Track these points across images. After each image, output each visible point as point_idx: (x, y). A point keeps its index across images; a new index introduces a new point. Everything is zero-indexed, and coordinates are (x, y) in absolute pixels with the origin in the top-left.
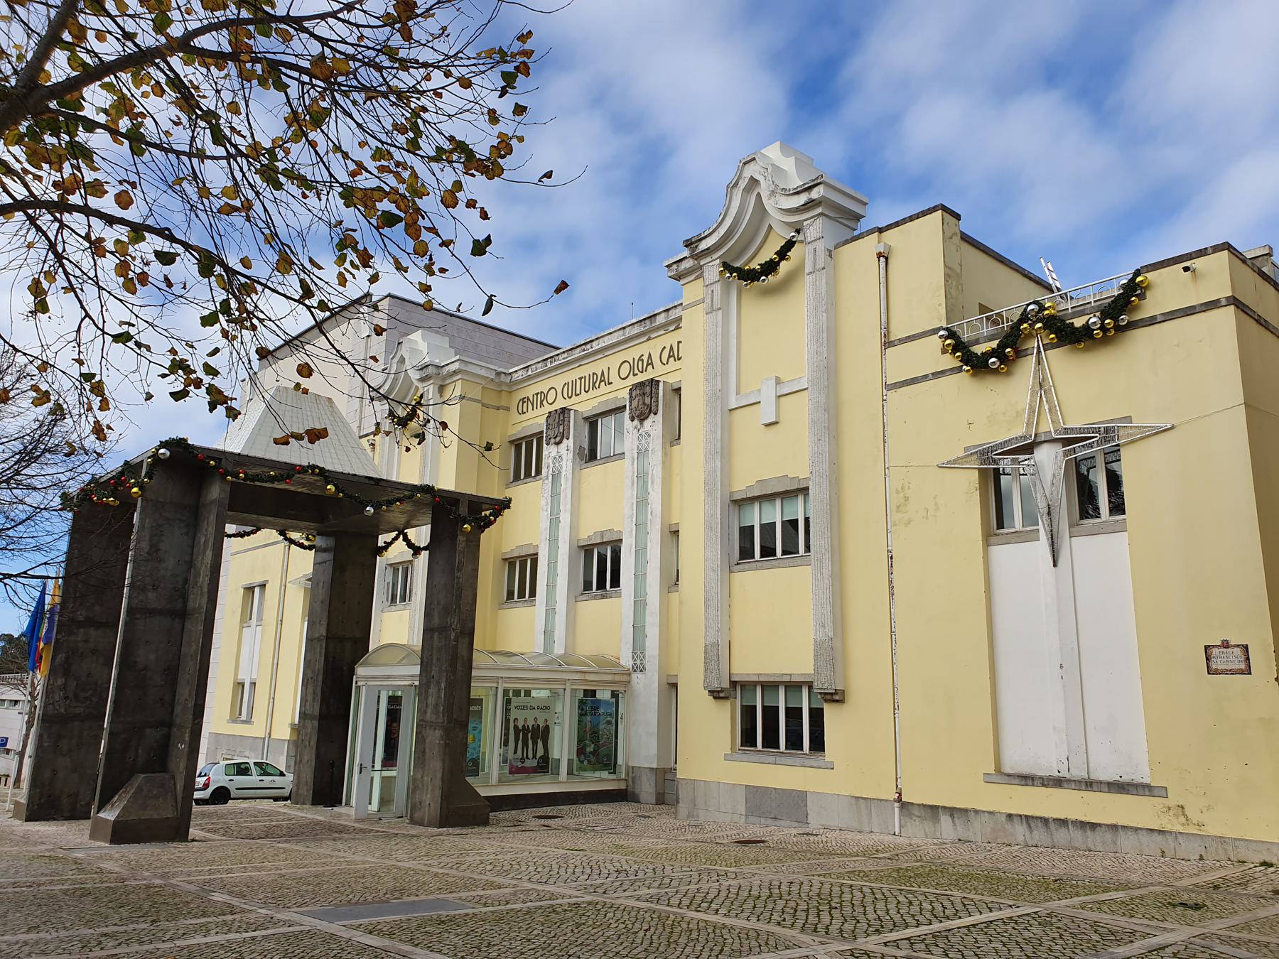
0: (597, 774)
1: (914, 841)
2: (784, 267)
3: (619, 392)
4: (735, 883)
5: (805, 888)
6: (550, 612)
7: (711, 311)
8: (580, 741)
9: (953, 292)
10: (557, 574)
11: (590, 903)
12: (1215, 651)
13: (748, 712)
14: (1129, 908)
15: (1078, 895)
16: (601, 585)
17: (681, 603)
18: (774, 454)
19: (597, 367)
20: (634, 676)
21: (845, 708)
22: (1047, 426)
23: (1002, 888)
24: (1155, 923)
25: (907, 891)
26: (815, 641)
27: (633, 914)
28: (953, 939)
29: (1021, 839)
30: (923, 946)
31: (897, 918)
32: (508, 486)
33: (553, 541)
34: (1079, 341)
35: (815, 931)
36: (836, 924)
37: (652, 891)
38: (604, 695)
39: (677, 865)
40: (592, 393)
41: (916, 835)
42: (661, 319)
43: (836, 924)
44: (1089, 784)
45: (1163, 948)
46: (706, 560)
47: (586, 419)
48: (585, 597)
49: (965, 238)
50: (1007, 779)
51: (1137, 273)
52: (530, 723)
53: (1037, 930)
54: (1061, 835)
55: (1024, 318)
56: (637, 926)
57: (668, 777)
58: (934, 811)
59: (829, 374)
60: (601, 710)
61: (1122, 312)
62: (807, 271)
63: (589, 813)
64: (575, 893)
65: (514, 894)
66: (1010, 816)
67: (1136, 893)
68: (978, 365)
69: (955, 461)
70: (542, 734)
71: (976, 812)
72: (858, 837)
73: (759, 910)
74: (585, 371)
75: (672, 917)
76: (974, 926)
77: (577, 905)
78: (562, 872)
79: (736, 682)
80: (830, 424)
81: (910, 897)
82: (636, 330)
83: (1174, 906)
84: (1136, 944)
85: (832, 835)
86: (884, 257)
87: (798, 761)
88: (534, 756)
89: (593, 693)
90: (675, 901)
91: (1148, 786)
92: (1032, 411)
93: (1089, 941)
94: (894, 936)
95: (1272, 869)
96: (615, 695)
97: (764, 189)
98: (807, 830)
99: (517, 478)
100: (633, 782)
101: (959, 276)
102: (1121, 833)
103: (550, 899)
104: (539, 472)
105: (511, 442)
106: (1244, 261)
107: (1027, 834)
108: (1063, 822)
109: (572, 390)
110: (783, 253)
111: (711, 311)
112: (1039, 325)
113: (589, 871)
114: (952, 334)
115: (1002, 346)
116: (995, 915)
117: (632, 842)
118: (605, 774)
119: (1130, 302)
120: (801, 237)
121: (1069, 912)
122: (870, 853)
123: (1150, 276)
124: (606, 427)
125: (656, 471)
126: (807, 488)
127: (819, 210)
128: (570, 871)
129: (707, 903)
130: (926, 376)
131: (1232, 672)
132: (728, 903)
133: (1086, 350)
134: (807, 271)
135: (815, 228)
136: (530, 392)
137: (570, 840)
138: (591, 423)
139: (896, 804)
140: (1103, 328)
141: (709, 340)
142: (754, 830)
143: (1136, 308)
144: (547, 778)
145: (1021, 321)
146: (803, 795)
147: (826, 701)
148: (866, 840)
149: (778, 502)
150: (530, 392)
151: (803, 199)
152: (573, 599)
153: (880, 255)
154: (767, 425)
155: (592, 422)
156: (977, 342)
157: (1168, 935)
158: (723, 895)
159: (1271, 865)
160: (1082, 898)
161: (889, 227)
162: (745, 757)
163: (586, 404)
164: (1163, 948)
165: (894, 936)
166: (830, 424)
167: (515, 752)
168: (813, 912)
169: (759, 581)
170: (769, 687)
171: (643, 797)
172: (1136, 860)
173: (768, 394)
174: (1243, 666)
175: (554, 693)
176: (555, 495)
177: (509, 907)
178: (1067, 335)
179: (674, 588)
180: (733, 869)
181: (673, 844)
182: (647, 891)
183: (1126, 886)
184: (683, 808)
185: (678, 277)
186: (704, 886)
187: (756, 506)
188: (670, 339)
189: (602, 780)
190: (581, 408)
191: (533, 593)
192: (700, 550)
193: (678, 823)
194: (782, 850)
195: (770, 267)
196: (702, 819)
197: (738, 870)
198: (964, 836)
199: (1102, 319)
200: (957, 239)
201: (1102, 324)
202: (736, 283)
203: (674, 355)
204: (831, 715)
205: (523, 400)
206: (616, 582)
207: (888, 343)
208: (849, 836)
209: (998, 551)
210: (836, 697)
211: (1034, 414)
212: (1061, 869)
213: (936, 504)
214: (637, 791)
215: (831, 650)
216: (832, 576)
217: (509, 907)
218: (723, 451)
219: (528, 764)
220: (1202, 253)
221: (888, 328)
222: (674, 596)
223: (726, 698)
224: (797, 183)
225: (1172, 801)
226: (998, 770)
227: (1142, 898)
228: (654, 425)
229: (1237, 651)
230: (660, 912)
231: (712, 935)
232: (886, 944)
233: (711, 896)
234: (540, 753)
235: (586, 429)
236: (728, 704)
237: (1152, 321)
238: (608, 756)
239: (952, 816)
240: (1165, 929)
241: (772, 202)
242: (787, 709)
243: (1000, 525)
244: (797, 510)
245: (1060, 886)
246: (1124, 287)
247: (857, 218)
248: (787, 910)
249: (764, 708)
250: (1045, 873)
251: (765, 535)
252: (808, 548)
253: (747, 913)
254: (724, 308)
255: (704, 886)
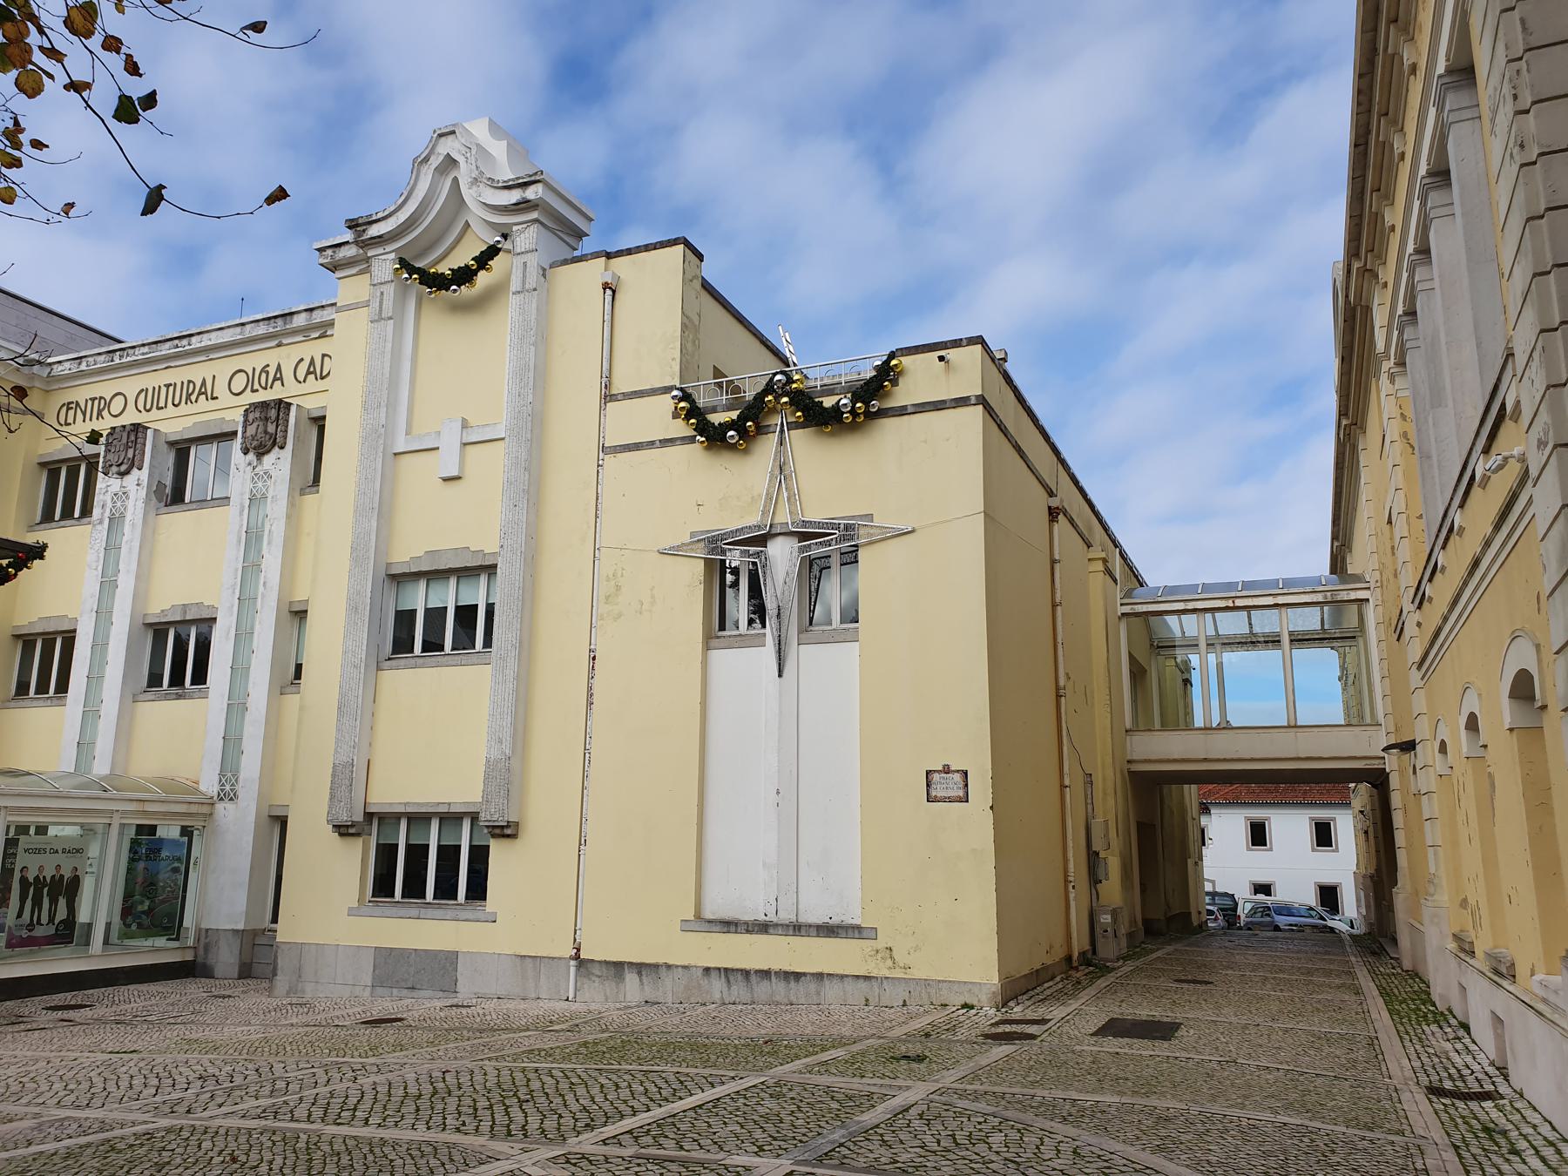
0: (149, 942)
1: (593, 1007)
2: (483, 278)
3: (229, 411)
4: (379, 1078)
5: (478, 1078)
6: (90, 714)
7: (379, 318)
8: (128, 896)
9: (689, 346)
10: (106, 662)
11: (169, 1130)
12: (936, 777)
13: (386, 854)
14: (854, 1065)
15: (797, 1057)
16: (177, 679)
17: (302, 708)
18: (435, 526)
19: (197, 372)
20: (220, 806)
21: (517, 844)
22: (783, 517)
23: (713, 1057)
24: (887, 1081)
25: (607, 1071)
26: (488, 761)
27: (242, 1139)
28: (682, 1127)
29: (717, 996)
30: (649, 1140)
31: (607, 1106)
32: (31, 528)
33: (103, 615)
34: (826, 424)
35: (509, 1134)
36: (534, 1122)
37: (263, 1102)
38: (169, 832)
39: (290, 1061)
40: (190, 408)
41: (595, 998)
42: (300, 321)
43: (534, 1122)
44: (797, 929)
45: (906, 1110)
46: (345, 653)
47: (171, 444)
48: (149, 696)
49: (706, 286)
50: (706, 926)
51: (892, 356)
52: (49, 873)
53: (770, 1104)
54: (762, 989)
55: (769, 388)
56: (254, 1156)
57: (260, 940)
58: (617, 968)
59: (533, 426)
60: (164, 854)
61: (872, 397)
62: (513, 289)
63: (135, 998)
64: (146, 1117)
65: (39, 1127)
66: (707, 970)
67: (855, 1048)
68: (714, 437)
69: (678, 548)
70: (69, 888)
71: (669, 967)
72: (523, 1005)
73: (425, 1114)
74: (178, 375)
75: (304, 1137)
76: (700, 1106)
77: (150, 1135)
78: (111, 1087)
79: (372, 814)
80: (530, 488)
81: (614, 1077)
82: (262, 330)
83: (898, 1060)
84: (880, 1108)
85: (490, 1006)
86: (610, 288)
87: (450, 913)
88: (51, 920)
89: (152, 829)
90: (301, 1112)
91: (858, 928)
92: (769, 497)
93: (830, 1110)
94: (610, 1130)
95: (973, 1012)
96: (187, 832)
97: (464, 174)
98: (455, 1001)
99: (48, 517)
100: (207, 948)
101: (697, 330)
102: (827, 982)
103: (102, 1130)
104: (87, 511)
105: (43, 465)
106: (993, 360)
107: (725, 990)
108: (765, 974)
109: (151, 398)
110: (484, 260)
111: (379, 318)
112: (785, 399)
113: (155, 1082)
114: (686, 396)
115: (743, 418)
116: (719, 1091)
117: (209, 1034)
118: (161, 942)
119: (883, 387)
120: (507, 245)
121: (797, 1078)
122: (545, 1025)
123: (906, 361)
124: (202, 462)
125: (276, 527)
126: (495, 566)
127: (535, 215)
128: (124, 1084)
129: (349, 1111)
130: (652, 443)
131: (951, 800)
132: (378, 1107)
133: (832, 434)
134: (513, 289)
135: (527, 237)
136: (81, 394)
137: (112, 1039)
138: (178, 450)
139: (573, 963)
140: (853, 412)
141: (355, 359)
142: (385, 1005)
143: (887, 395)
144: (64, 951)
145: (766, 392)
146: (451, 958)
147: (494, 836)
148: (535, 1010)
149: (453, 581)
150: (81, 394)
151: (514, 196)
152: (131, 698)
153: (606, 286)
154: (446, 480)
155: (181, 450)
156: (714, 410)
157: (906, 1094)
158: (368, 1098)
159: (972, 1007)
160: (805, 1061)
161: (620, 253)
162: (378, 911)
163: (174, 423)
164: (906, 1110)
165: (610, 1130)
166: (530, 488)
167: (19, 915)
168: (499, 1109)
169: (421, 685)
170: (418, 819)
171: (218, 972)
172: (840, 1011)
173: (450, 441)
174: (961, 793)
175: (88, 830)
176: (111, 548)
177: (34, 1149)
178: (816, 415)
179: (293, 688)
180: (372, 1060)
181: (273, 1032)
182: (256, 1103)
183: (840, 1042)
184: (282, 983)
185: (334, 267)
186: (340, 1088)
187: (422, 584)
188: (313, 349)
189: (159, 950)
190: (165, 428)
191: (63, 687)
192: (335, 639)
193: (275, 1002)
194: (430, 1029)
195: (464, 276)
196: (308, 996)
197: (379, 1062)
198: (652, 998)
199: (854, 402)
200: (697, 284)
201: (853, 407)
202: (417, 287)
203: (316, 371)
204: (499, 853)
205: (68, 406)
206: (200, 676)
207: (608, 397)
208: (511, 1005)
209: (717, 656)
210: (507, 832)
211: (772, 501)
212: (769, 1029)
213: (653, 597)
214: (211, 960)
215: (506, 773)
216: (517, 678)
217: (34, 1149)
218: (381, 508)
219: (39, 932)
220: (956, 344)
221: (609, 377)
222: (292, 701)
223: (358, 835)
224: (507, 174)
225: (881, 943)
226: (698, 916)
227: (863, 1053)
228: (279, 463)
229: (957, 777)
230: (284, 1131)
231: (370, 1158)
232: (604, 1142)
233: (352, 1101)
234: (62, 914)
235: (170, 459)
236: (359, 842)
237: (902, 411)
238: (171, 916)
239: (640, 974)
240: (900, 1088)
241: (473, 191)
242: (440, 847)
243: (722, 627)
244: (476, 594)
245: (771, 1048)
246: (877, 368)
247: (580, 235)
248: (463, 1109)
249: (409, 847)
250: (753, 1034)
251: (433, 621)
252: (488, 643)
253: (409, 1120)
254: (397, 317)
255: (340, 1088)
